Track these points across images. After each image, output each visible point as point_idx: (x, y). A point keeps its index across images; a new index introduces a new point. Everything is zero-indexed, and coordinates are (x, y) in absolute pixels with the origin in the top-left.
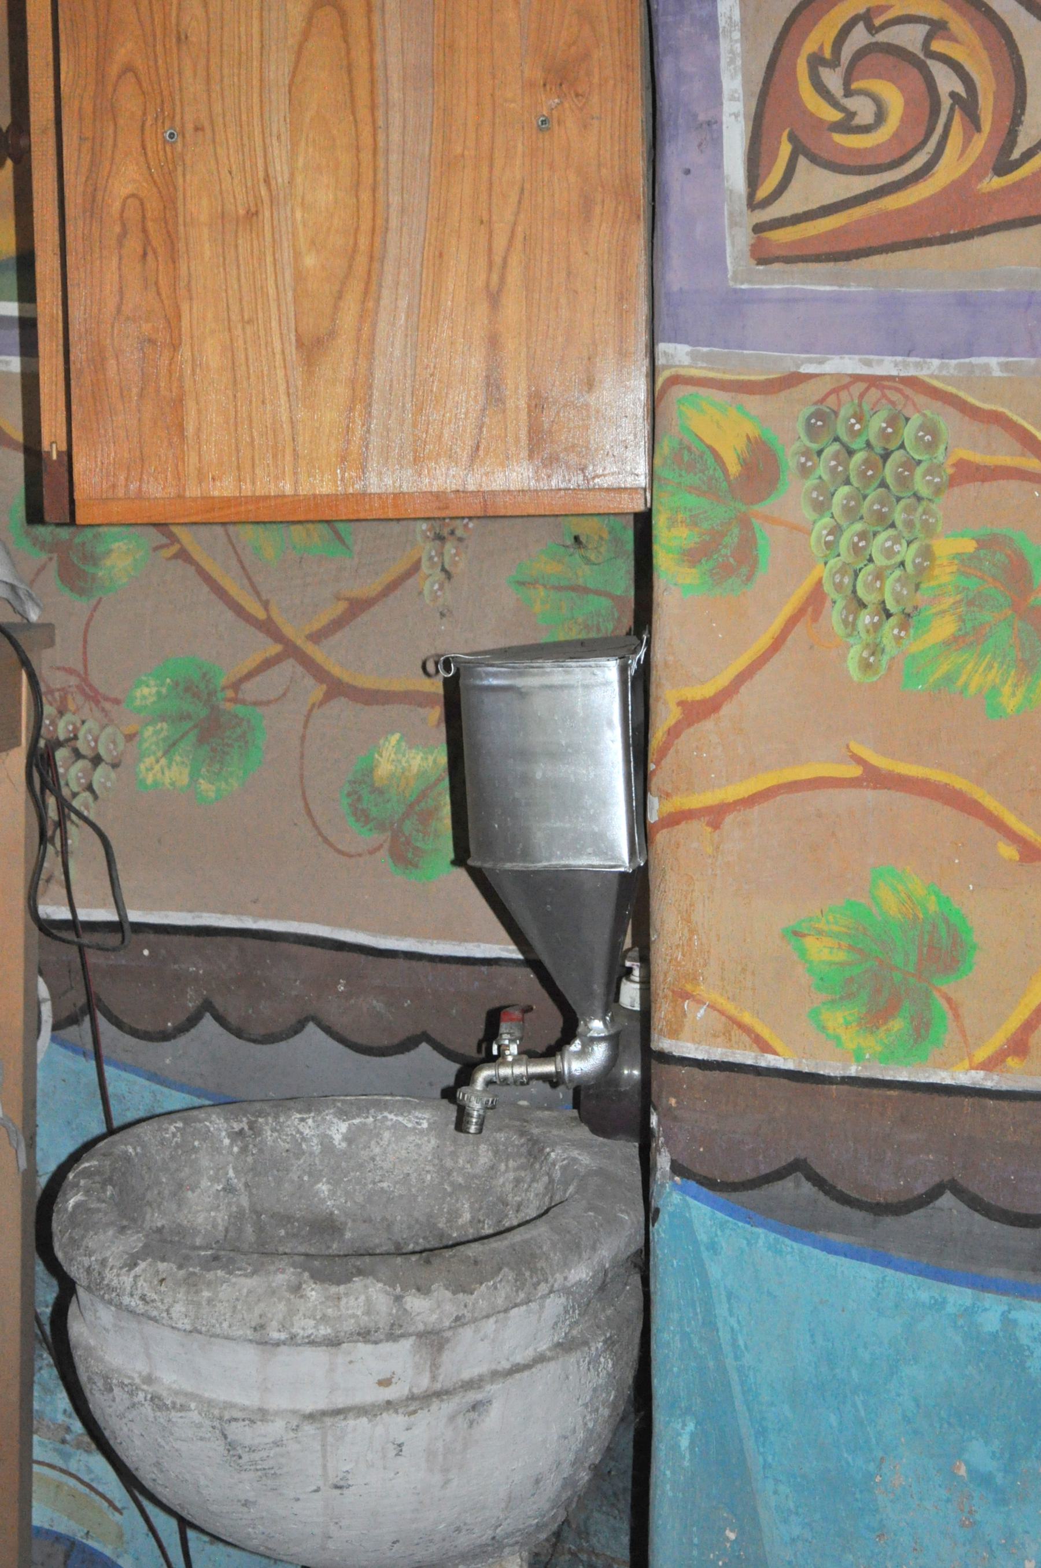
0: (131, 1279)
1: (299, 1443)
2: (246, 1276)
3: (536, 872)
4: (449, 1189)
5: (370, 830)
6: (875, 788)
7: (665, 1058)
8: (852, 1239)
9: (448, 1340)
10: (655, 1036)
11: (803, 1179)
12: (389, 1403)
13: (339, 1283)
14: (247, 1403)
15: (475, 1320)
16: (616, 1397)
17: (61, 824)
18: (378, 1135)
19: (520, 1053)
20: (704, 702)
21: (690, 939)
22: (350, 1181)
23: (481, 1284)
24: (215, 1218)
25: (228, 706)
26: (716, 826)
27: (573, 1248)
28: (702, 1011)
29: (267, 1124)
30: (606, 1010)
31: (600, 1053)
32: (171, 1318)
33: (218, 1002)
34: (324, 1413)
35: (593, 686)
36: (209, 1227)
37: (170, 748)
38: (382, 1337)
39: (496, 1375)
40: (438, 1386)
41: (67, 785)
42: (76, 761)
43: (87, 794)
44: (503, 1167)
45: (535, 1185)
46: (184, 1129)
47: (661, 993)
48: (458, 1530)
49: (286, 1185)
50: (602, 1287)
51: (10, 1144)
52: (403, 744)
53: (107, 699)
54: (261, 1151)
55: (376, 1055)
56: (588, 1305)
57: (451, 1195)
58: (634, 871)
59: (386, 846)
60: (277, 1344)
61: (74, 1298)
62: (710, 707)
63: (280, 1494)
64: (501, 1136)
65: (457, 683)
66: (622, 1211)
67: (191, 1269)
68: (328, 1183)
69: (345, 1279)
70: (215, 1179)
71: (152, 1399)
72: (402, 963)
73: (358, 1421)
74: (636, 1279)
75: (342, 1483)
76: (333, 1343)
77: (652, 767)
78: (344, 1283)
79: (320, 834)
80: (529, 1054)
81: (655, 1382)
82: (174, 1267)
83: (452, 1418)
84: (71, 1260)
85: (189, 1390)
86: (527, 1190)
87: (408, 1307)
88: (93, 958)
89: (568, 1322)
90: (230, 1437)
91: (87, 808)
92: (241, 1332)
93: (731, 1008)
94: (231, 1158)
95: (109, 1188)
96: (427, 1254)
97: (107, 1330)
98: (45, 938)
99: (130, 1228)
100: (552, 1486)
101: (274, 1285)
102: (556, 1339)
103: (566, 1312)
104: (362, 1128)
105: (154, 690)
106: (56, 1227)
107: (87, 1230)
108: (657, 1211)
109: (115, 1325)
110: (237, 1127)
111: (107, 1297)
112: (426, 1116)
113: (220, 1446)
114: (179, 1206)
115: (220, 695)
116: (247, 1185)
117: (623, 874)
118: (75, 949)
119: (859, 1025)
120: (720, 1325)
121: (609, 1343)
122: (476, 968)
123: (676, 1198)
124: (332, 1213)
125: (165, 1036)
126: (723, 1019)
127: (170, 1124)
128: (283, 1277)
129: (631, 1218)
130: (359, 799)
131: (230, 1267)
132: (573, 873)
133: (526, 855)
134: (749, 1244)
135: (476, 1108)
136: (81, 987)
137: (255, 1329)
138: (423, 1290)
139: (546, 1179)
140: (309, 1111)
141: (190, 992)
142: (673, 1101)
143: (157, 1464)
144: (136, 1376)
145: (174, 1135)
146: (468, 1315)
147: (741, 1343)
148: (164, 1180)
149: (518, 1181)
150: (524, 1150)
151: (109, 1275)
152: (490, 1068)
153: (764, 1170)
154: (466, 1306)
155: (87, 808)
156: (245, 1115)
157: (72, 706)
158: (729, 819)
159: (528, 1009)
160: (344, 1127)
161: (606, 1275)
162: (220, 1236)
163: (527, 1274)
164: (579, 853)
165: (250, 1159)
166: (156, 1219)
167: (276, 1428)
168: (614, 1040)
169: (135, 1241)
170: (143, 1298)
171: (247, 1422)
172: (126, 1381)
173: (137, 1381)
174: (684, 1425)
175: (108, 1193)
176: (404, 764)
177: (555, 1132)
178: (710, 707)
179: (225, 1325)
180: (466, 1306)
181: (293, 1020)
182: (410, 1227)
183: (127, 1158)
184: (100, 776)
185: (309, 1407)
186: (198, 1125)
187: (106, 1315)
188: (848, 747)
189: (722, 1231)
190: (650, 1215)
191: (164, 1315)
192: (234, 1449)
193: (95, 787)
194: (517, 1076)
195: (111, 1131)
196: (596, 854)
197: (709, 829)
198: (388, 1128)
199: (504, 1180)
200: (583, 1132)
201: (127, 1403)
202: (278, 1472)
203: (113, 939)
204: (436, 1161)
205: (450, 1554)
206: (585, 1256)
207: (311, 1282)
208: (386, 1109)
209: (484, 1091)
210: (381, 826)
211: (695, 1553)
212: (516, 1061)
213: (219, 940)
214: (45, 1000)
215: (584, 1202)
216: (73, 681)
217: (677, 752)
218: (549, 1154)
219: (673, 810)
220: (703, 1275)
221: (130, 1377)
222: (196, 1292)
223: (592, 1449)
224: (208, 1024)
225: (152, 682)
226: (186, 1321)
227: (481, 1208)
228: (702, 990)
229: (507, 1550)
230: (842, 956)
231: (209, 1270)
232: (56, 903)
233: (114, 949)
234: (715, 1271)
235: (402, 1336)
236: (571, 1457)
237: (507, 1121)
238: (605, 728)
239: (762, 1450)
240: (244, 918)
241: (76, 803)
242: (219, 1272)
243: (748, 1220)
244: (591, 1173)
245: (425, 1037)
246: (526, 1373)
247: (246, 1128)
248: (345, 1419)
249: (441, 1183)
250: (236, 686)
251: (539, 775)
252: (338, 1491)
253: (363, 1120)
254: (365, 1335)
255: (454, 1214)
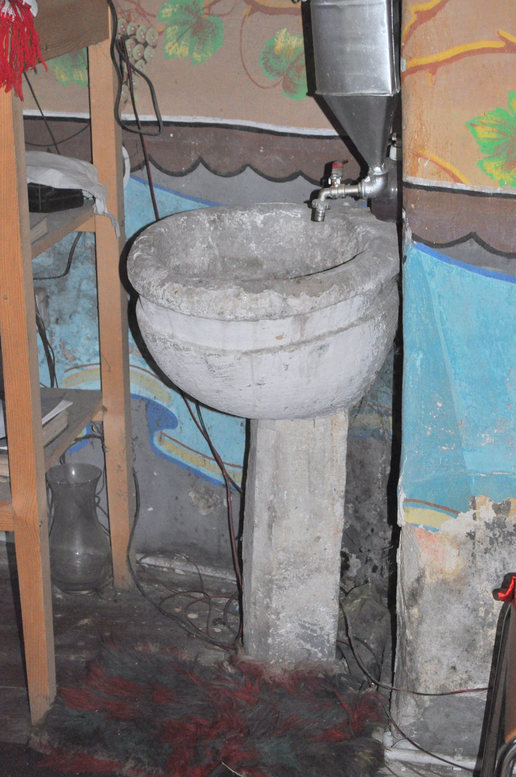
0: (162, 291)
1: (241, 365)
2: (214, 290)
3: (347, 97)
4: (311, 245)
5: (274, 75)
6: (511, 53)
7: (409, 185)
8: (497, 270)
9: (308, 318)
10: (404, 174)
11: (474, 242)
12: (281, 346)
13: (257, 293)
14: (217, 347)
15: (321, 309)
16: (387, 341)
17: (129, 76)
18: (278, 221)
19: (341, 182)
20: (428, 11)
21: (421, 128)
22: (265, 242)
23: (323, 292)
24: (203, 260)
25: (206, 17)
26: (434, 73)
27: (367, 274)
28: (427, 163)
29: (226, 216)
30: (382, 162)
31: (379, 183)
32: (181, 309)
33: (206, 159)
34: (252, 352)
35: (374, 5)
36: (201, 265)
37: (180, 37)
38: (277, 317)
39: (331, 333)
40: (304, 339)
41: (132, 56)
42: (136, 45)
43: (142, 61)
44: (335, 235)
45: (350, 243)
46: (187, 219)
47: (407, 154)
48: (315, 402)
49: (236, 244)
50: (381, 291)
51: (112, 225)
52: (288, 34)
53: (150, 15)
54: (224, 229)
55: (279, 182)
56: (374, 300)
57: (312, 248)
58: (394, 96)
59: (281, 83)
60: (230, 321)
61: (138, 299)
62: (431, 14)
63: (233, 388)
64: (335, 221)
65: (309, 5)
66: (390, 256)
67: (189, 287)
68: (255, 243)
69: (260, 291)
70: (202, 243)
71: (174, 345)
72: (288, 138)
73: (267, 355)
74: (396, 288)
75: (260, 383)
76: (255, 320)
77: (403, 44)
78: (259, 293)
79: (250, 78)
80: (346, 182)
81: (405, 336)
82: (182, 286)
83: (311, 353)
84: (135, 282)
85: (191, 341)
86: (347, 246)
87: (289, 303)
88: (146, 138)
89: (364, 308)
90: (210, 363)
91: (142, 67)
92: (212, 316)
93: (440, 161)
94: (210, 233)
95: (153, 248)
96: (298, 279)
97: (153, 314)
98: (125, 131)
99: (161, 268)
100: (358, 382)
101: (227, 294)
102: (359, 316)
103: (364, 303)
104: (270, 217)
105: (171, 10)
106: (128, 267)
107: (142, 268)
108: (406, 257)
109: (156, 312)
110: (212, 218)
111: (151, 299)
112: (300, 211)
113: (205, 367)
114: (186, 255)
115: (202, 12)
116: (217, 245)
117: (389, 98)
118: (138, 135)
119: (502, 168)
120: (435, 310)
121: (384, 317)
122: (324, 140)
123: (414, 251)
124: (257, 257)
125: (181, 174)
126: (437, 167)
127: (181, 217)
128: (231, 291)
129: (394, 259)
130: (268, 61)
131: (207, 285)
132: (364, 98)
133: (343, 88)
134: (448, 272)
135: (321, 210)
136: (141, 152)
137: (219, 314)
138: (296, 295)
139: (355, 241)
140: (245, 210)
141: (193, 153)
142: (413, 206)
143: (178, 374)
144: (166, 335)
145: (183, 222)
146: (318, 307)
147: (445, 318)
148: (179, 243)
149: (342, 242)
150: (345, 227)
151: (152, 290)
152: (327, 190)
153: (456, 238)
154: (316, 302)
155: (142, 67)
156: (216, 213)
157: (133, 18)
158: (440, 70)
159: (345, 162)
160: (262, 217)
161: (382, 285)
162: (206, 268)
163: (345, 287)
164: (367, 87)
165: (219, 233)
166: (175, 262)
167: (230, 359)
168: (386, 177)
169: (164, 273)
170: (168, 300)
171: (217, 356)
172: (162, 337)
173: (167, 337)
174: (418, 355)
175: (152, 251)
176: (289, 44)
177: (360, 218)
178: (431, 14)
179: (205, 312)
180: (316, 302)
181: (240, 166)
182: (293, 263)
183: (161, 234)
184: (148, 52)
185: (245, 349)
186: (194, 218)
187: (152, 307)
188: (498, 32)
189: (436, 266)
190: (402, 259)
191: (178, 308)
192: (211, 368)
193: (145, 57)
194: (340, 194)
195: (158, 220)
196: (377, 87)
197: (430, 74)
198: (282, 218)
199: (336, 241)
200: (373, 218)
201: (163, 347)
202: (232, 378)
203: (156, 130)
204: (305, 233)
205: (312, 412)
206: (372, 278)
207: (244, 292)
208: (281, 208)
209: (325, 201)
210: (278, 74)
211: (423, 412)
212: (340, 187)
213: (204, 129)
214: (127, 158)
215: (372, 252)
216: (133, 6)
217: (415, 36)
218: (356, 229)
219: (413, 65)
220: (428, 288)
221: (164, 336)
222: (192, 298)
223: (376, 365)
224: (201, 168)
225: (170, 6)
226: (187, 310)
227: (325, 254)
228: (427, 153)
229: (338, 409)
230: (494, 135)
231: (197, 287)
232: (129, 113)
233: (156, 135)
234: (432, 285)
235: (287, 316)
236: (367, 369)
237: (337, 213)
238: (380, 26)
239: (454, 366)
240: (216, 118)
241: (137, 66)
242: (202, 288)
243: (448, 261)
244: (375, 238)
245: (301, 173)
246: (345, 332)
247: (216, 218)
248: (261, 354)
249: (307, 243)
250: (209, 7)
251: (348, 49)
252: (259, 386)
253: (270, 214)
254: (270, 316)
255: (313, 257)
